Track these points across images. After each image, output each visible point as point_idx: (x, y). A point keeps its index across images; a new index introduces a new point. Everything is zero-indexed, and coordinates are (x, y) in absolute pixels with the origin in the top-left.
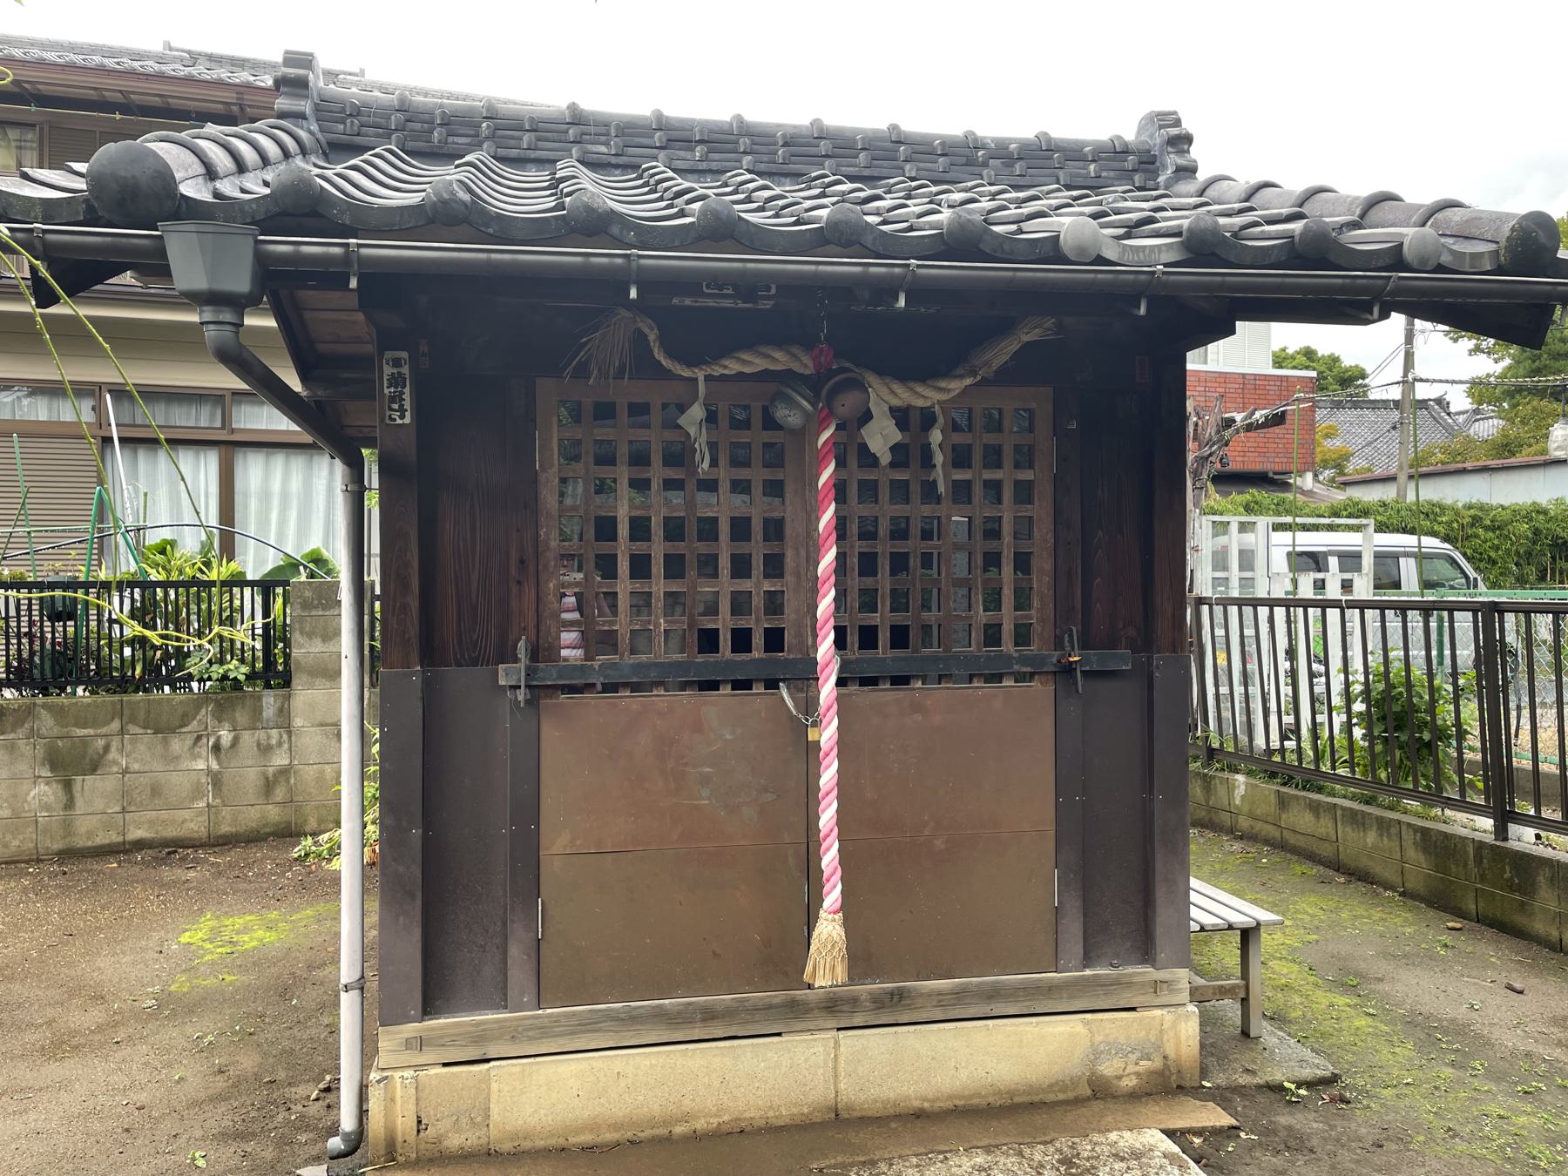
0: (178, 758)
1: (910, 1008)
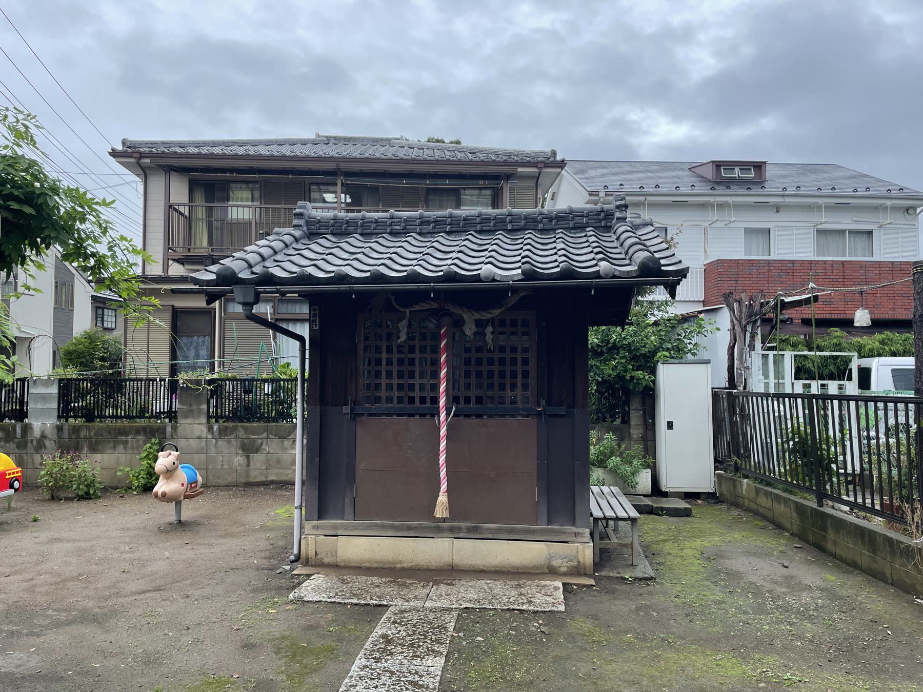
0: (286, 449)
1: (480, 533)
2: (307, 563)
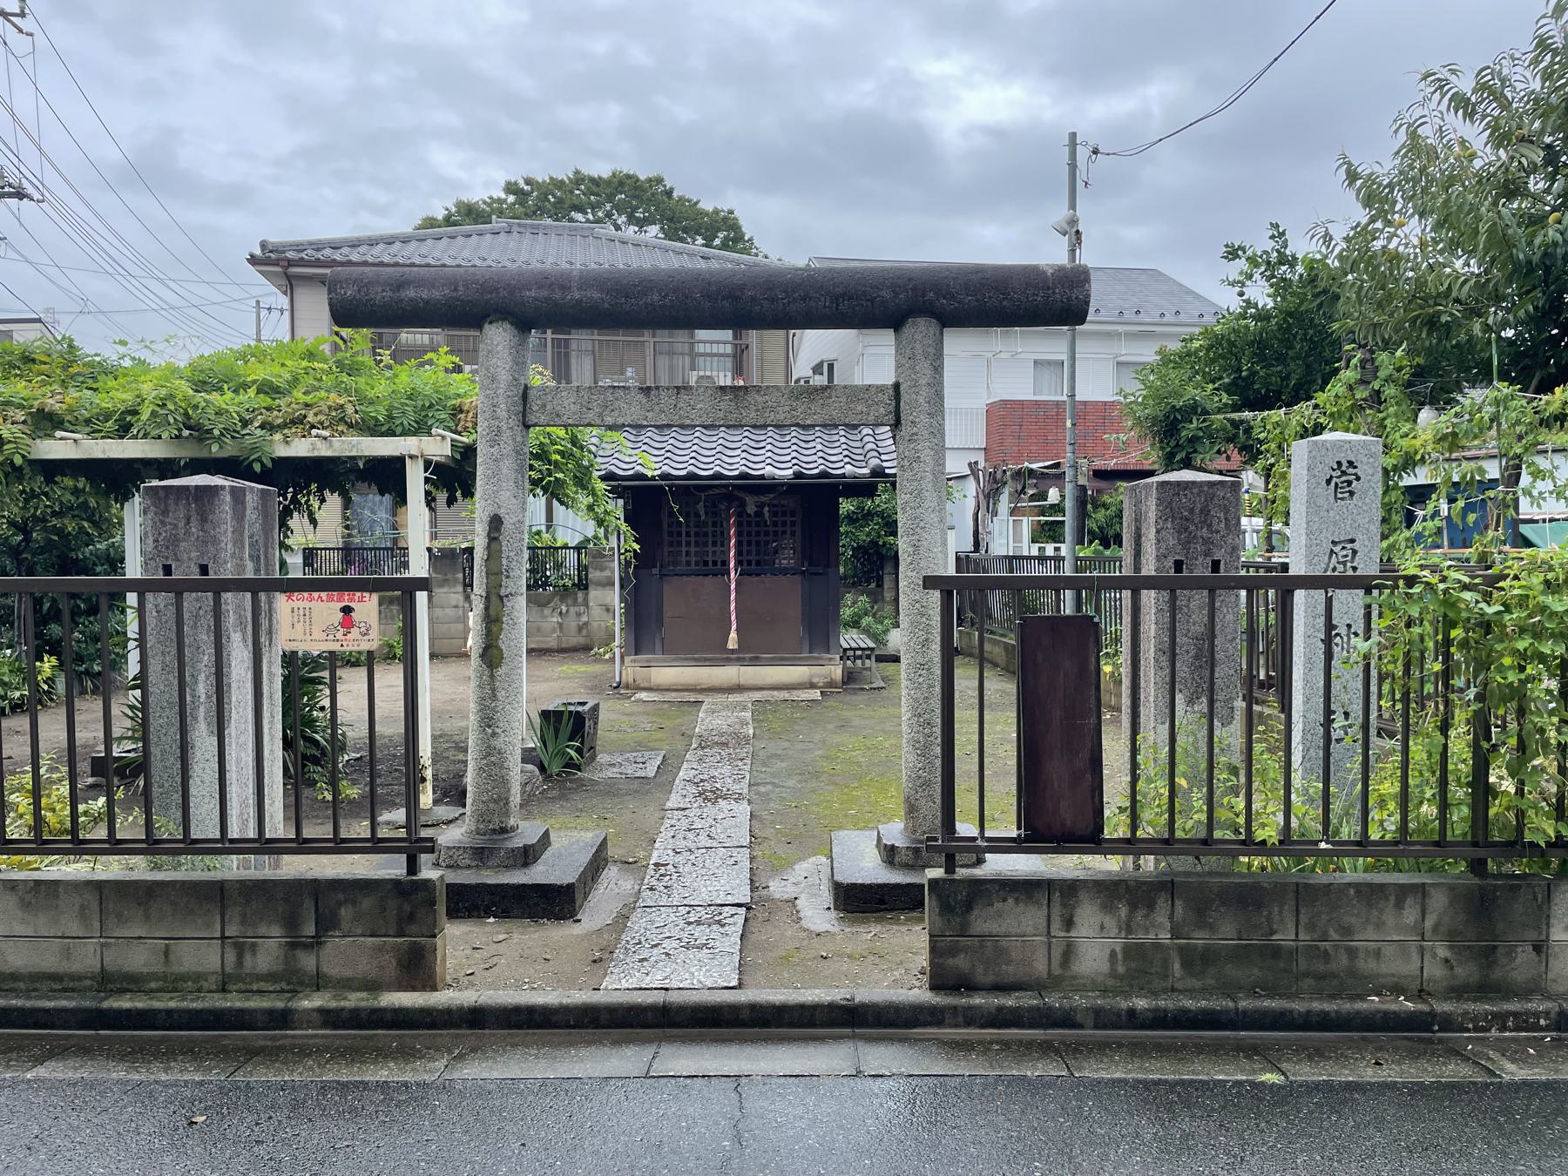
2: (627, 687)
